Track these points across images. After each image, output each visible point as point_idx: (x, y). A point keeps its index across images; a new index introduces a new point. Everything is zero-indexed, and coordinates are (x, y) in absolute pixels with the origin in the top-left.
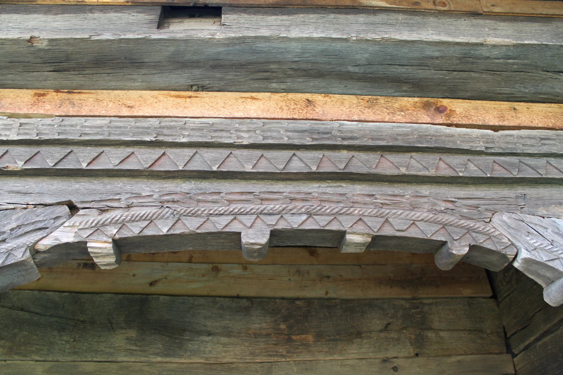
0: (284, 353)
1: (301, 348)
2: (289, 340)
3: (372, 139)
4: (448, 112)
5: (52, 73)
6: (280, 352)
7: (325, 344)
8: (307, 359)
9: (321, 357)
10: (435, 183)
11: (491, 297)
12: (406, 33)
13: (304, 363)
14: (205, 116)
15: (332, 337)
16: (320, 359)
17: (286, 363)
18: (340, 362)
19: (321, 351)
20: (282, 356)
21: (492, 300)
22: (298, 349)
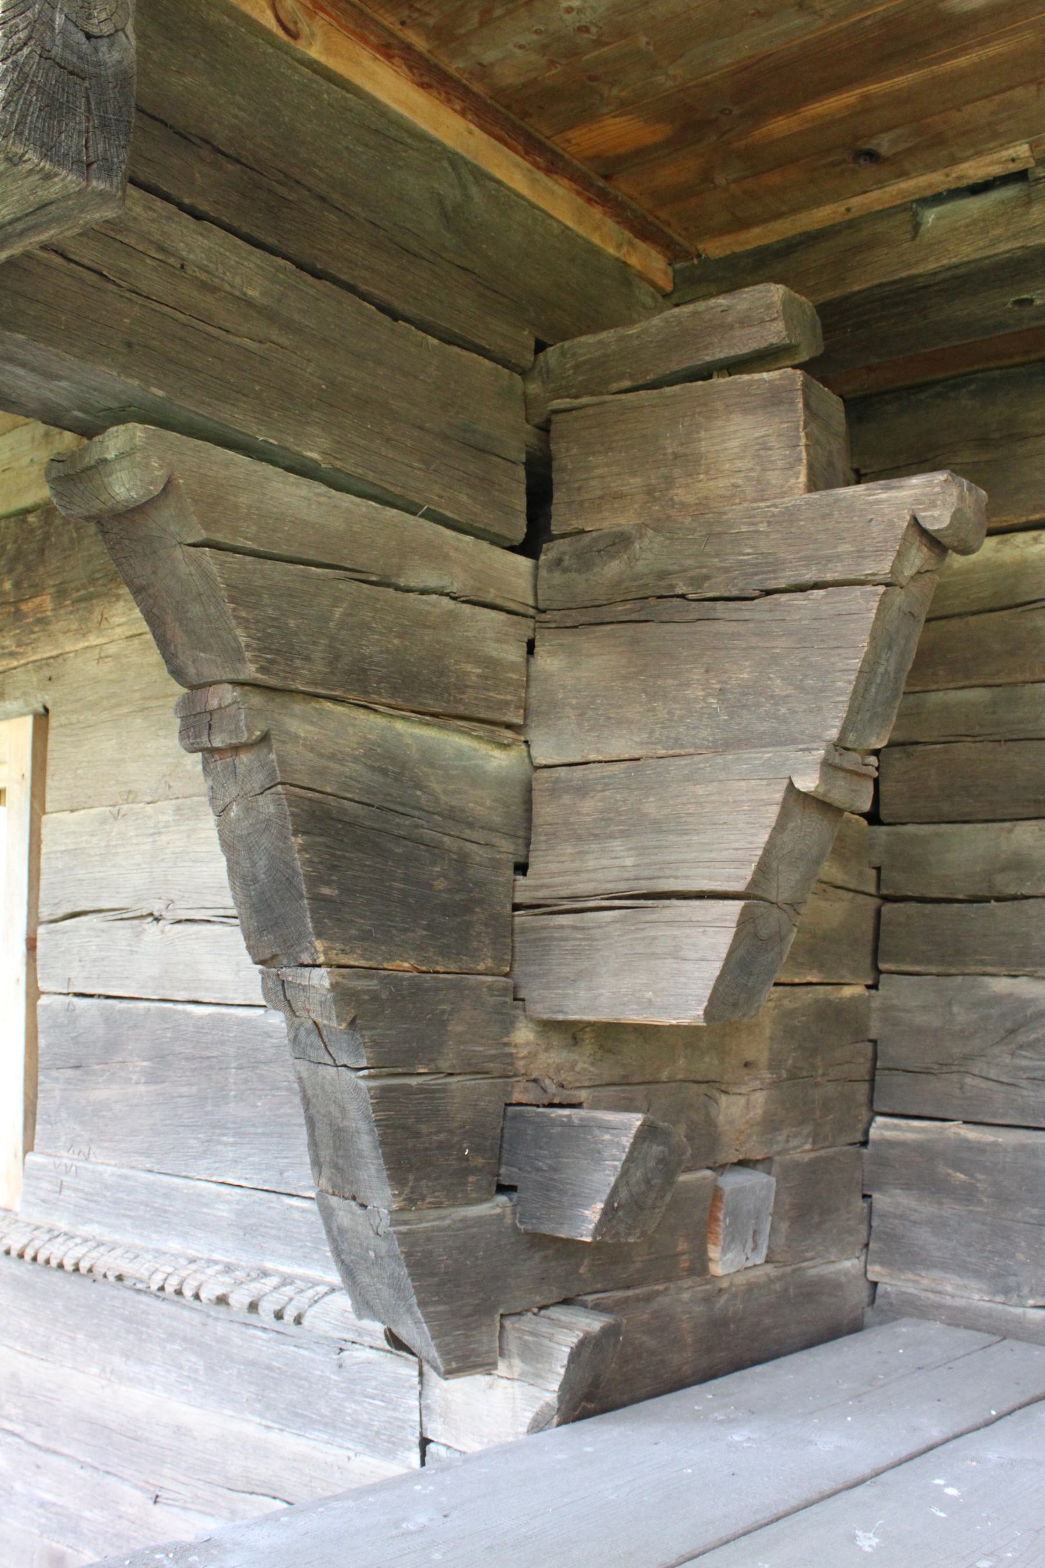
0: (13, 648)
1: (36, 629)
2: (18, 615)
4: (708, 1277)
5: (922, 740)
6: (7, 647)
7: (71, 612)
8: (49, 654)
9: (70, 646)
10: (1035, 1343)
11: (431, 1441)
13: (48, 665)
15: (83, 592)
16: (67, 650)
17: (22, 669)
18: (97, 651)
19: (69, 631)
20: (12, 655)
21: (430, 1437)
22: (33, 633)
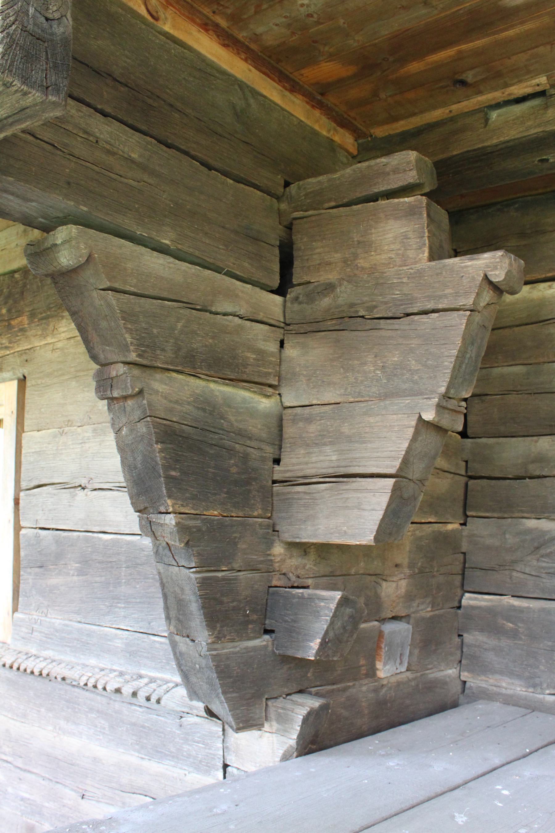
0: (7, 344)
1: (19, 334)
2: (9, 327)
3: (294, 102)
6: (4, 344)
7: (38, 325)
8: (26, 348)
9: (37, 343)
11: (229, 766)
12: (460, 107)
13: (25, 353)
14: (272, 697)
15: (44, 315)
16: (36, 345)
17: (12, 355)
18: (51, 346)
19: (36, 335)
20: (6, 348)
21: (228, 763)
22: (18, 336)
